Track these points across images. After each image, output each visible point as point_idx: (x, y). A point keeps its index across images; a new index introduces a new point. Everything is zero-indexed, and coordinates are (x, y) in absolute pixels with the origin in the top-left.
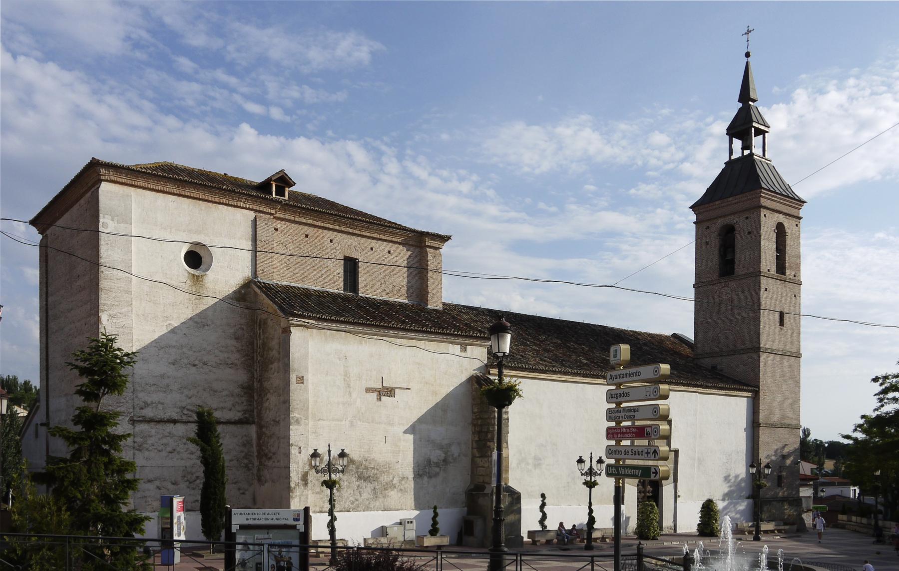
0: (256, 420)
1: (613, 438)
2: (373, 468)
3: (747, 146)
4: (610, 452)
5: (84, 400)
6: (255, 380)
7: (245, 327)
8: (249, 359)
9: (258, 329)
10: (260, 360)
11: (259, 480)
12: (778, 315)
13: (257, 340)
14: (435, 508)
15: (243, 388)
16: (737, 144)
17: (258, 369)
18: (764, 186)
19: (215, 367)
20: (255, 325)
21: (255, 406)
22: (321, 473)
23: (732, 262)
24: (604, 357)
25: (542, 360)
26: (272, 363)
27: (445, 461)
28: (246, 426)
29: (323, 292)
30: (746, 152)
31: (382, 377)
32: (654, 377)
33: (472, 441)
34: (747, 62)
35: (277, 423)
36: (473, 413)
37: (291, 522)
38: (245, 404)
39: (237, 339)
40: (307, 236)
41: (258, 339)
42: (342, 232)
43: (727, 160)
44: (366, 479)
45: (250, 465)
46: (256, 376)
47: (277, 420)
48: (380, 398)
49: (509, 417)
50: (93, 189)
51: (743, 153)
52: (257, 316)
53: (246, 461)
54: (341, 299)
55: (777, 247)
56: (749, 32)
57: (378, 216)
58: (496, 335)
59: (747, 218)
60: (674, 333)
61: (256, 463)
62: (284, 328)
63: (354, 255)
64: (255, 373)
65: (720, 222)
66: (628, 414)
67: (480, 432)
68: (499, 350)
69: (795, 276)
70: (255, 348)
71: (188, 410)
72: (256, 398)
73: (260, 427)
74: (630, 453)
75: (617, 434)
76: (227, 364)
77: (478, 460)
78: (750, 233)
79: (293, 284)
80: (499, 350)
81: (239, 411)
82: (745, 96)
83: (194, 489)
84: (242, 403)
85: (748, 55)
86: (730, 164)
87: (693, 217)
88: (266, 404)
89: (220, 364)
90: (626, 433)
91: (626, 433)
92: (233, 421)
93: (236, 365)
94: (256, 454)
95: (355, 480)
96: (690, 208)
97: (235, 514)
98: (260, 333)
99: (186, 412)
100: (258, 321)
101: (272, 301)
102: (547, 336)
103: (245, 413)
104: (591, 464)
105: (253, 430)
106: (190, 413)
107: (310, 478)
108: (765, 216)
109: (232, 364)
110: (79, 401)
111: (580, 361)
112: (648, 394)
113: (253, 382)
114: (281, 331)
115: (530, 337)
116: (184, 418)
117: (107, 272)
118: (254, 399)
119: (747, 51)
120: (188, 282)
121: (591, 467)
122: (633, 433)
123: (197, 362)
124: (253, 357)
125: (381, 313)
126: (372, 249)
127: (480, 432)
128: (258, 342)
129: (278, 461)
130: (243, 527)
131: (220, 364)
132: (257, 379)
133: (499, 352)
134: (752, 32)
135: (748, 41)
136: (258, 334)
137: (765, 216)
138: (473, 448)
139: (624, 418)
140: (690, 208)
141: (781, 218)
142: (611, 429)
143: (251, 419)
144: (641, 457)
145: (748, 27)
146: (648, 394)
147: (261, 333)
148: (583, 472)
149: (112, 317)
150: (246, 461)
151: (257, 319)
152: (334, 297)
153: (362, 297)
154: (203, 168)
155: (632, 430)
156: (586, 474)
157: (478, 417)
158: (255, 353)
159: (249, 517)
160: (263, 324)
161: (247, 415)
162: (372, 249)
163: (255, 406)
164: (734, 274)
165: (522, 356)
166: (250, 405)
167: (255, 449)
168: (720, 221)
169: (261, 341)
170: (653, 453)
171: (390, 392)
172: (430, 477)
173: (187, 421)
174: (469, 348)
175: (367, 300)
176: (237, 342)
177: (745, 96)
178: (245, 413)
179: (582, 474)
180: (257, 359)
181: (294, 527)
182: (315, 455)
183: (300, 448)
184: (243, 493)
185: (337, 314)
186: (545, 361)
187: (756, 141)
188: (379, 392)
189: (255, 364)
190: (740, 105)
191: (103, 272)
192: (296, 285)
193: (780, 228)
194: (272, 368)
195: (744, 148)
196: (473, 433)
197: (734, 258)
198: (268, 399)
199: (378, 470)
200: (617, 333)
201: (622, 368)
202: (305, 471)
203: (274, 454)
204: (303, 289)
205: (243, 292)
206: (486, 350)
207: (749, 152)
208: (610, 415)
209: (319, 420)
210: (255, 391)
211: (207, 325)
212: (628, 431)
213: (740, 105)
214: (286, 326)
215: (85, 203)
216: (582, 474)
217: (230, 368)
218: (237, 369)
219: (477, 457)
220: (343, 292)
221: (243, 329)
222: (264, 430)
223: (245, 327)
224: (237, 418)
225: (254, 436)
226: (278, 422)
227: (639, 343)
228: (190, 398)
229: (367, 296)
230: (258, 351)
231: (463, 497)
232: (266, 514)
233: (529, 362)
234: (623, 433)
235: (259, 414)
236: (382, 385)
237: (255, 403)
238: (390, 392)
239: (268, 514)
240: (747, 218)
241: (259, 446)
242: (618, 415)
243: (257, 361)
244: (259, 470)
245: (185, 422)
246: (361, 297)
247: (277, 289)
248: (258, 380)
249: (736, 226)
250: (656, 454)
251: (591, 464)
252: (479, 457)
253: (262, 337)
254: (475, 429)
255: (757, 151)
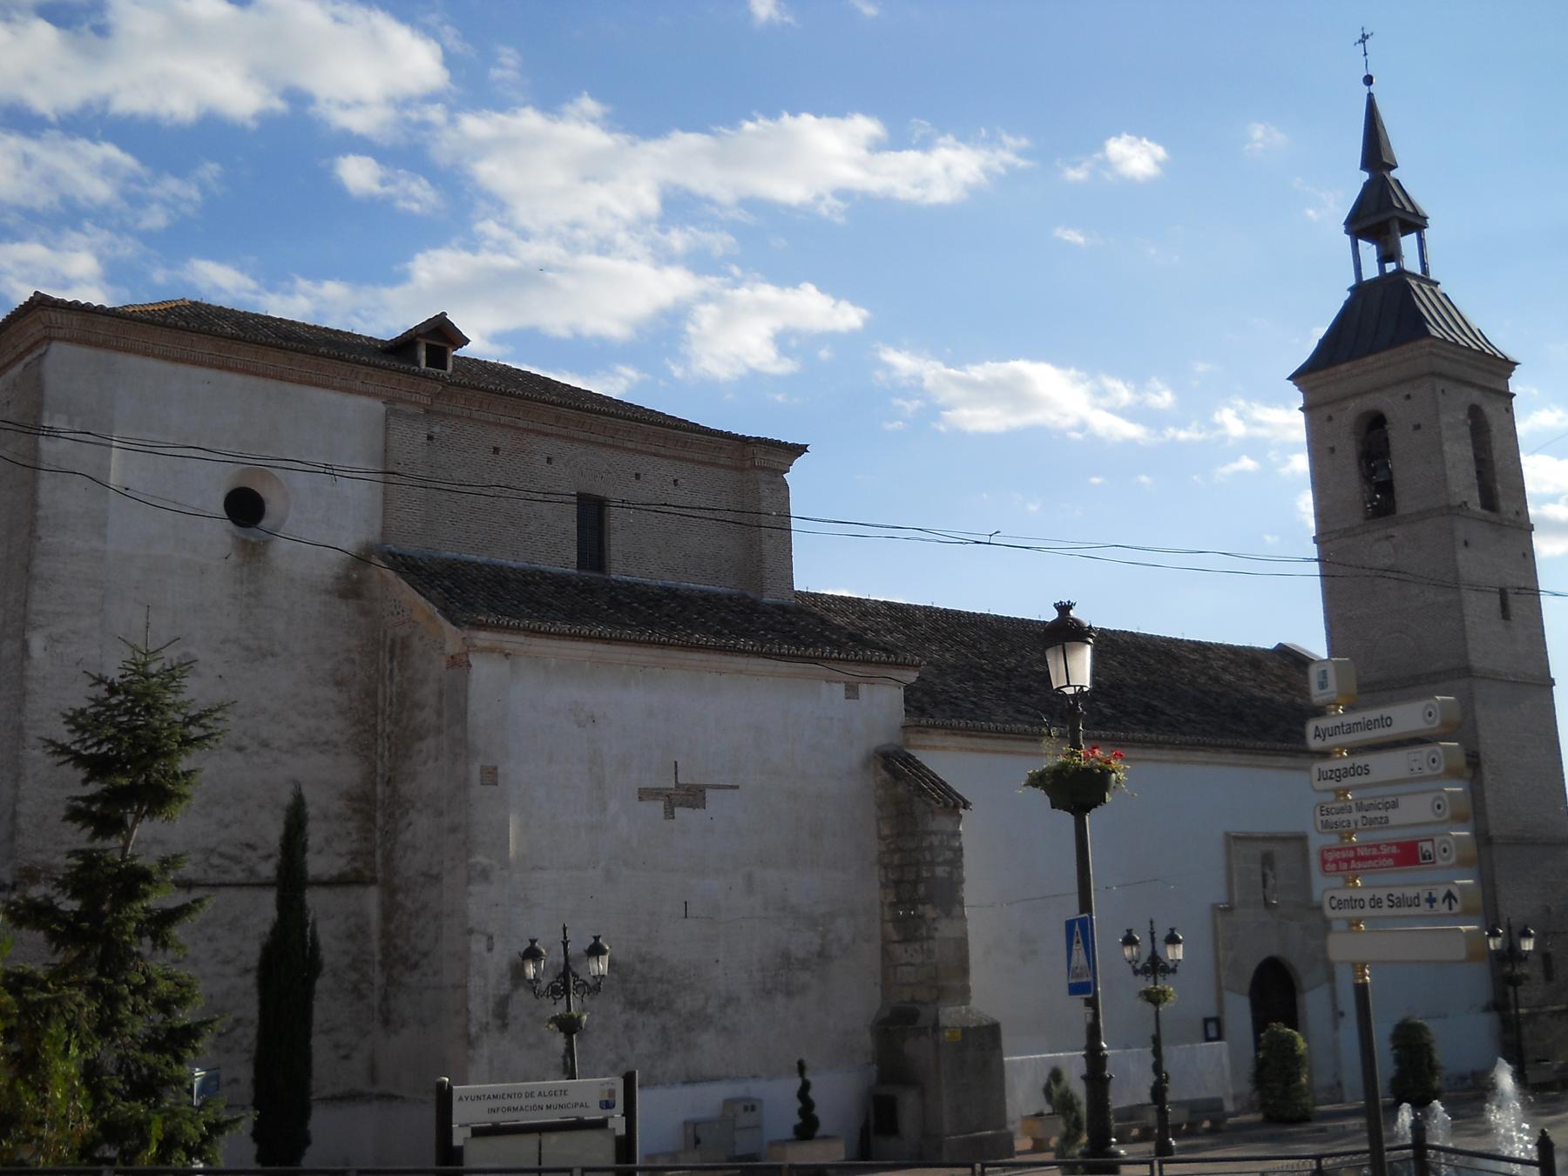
0: (380, 875)
1: (1338, 870)
2: (660, 980)
3: (1389, 254)
4: (1334, 903)
5: (95, 835)
6: (378, 779)
7: (357, 658)
8: (365, 731)
9: (387, 660)
10: (392, 732)
11: (386, 1022)
12: (1496, 600)
13: (385, 686)
14: (801, 1068)
15: (351, 799)
16: (1369, 251)
17: (386, 753)
18: (1434, 333)
19: (287, 752)
20: (381, 653)
21: (379, 841)
22: (548, 997)
23: (1387, 488)
24: (1146, 700)
25: (1019, 712)
26: (421, 739)
27: (823, 955)
28: (357, 891)
29: (533, 573)
30: (1390, 267)
31: (676, 763)
32: (1428, 726)
33: (882, 904)
34: (1370, 95)
35: (433, 879)
36: (881, 838)
37: (594, 1114)
38: (354, 837)
39: (339, 684)
40: (496, 450)
41: (388, 683)
42: (572, 439)
43: (1352, 282)
44: (644, 1006)
45: (363, 986)
46: (380, 771)
47: (434, 871)
48: (673, 813)
49: (963, 844)
50: (28, 359)
51: (1382, 269)
52: (385, 632)
53: (354, 976)
54: (575, 587)
55: (1475, 456)
56: (1365, 38)
57: (646, 407)
58: (1061, 646)
59: (1408, 397)
60: (1280, 644)
61: (378, 978)
62: (452, 657)
63: (598, 490)
64: (379, 763)
65: (1355, 407)
66: (1371, 814)
67: (898, 883)
68: (1068, 682)
69: (1517, 513)
70: (381, 704)
71: (221, 855)
72: (380, 821)
73: (390, 891)
74: (1386, 903)
75: (1348, 860)
76: (315, 744)
77: (898, 950)
78: (1417, 427)
79: (465, 556)
80: (1068, 682)
81: (340, 855)
82: (1376, 154)
83: (228, 1051)
84: (349, 834)
85: (1368, 80)
86: (1361, 290)
87: (1298, 399)
88: (406, 837)
89: (301, 744)
90: (1372, 858)
91: (1372, 858)
92: (325, 878)
93: (336, 746)
94: (378, 957)
95: (617, 1008)
96: (1289, 379)
97: (461, 1099)
98: (391, 671)
99: (215, 860)
100: (388, 642)
101: (424, 596)
102: (1019, 658)
103: (354, 859)
104: (1153, 947)
105: (371, 900)
106: (226, 863)
107: (514, 1010)
108: (1443, 391)
109: (326, 743)
110: (79, 837)
111: (1100, 712)
112: (1416, 766)
113: (374, 784)
114: (444, 664)
115: (983, 661)
116: (213, 876)
117: (50, 540)
118: (375, 826)
119: (1366, 74)
120: (233, 558)
121: (1154, 952)
122: (1388, 856)
123: (245, 742)
124: (375, 726)
125: (668, 615)
126: (638, 476)
127: (898, 883)
128: (388, 690)
129: (435, 973)
130: (478, 1132)
131: (301, 744)
132: (383, 776)
133: (1069, 685)
134: (1357, 41)
135: (1365, 54)
136: (388, 672)
137: (1443, 391)
138: (883, 921)
139: (1360, 823)
140: (1289, 379)
141: (1475, 396)
142: (1329, 851)
143: (367, 873)
144: (1413, 911)
145: (1363, 29)
146: (1416, 766)
147: (396, 671)
148: (1139, 966)
149: (54, 640)
150: (354, 976)
151: (385, 636)
152: (560, 583)
153: (619, 582)
154: (267, 312)
155: (1385, 851)
156: (1144, 971)
157: (892, 846)
158: (379, 717)
159: (493, 1104)
160: (399, 649)
161: (358, 865)
162: (638, 476)
163: (379, 841)
164: (1395, 513)
165: (973, 703)
166: (366, 839)
167: (375, 945)
168: (1353, 405)
169: (394, 689)
170: (1444, 901)
171: (693, 796)
172: (789, 994)
173: (217, 882)
174: (863, 688)
175: (631, 587)
176: (341, 691)
177: (1376, 154)
178: (354, 859)
179: (1136, 972)
180: (384, 731)
181: (601, 1125)
182: (532, 954)
183: (490, 938)
184: (347, 1057)
185: (571, 617)
186: (1027, 713)
187: (1408, 243)
188: (668, 796)
189: (380, 742)
190: (1366, 176)
191: (40, 538)
192: (473, 557)
193: (1475, 412)
194: (421, 751)
195: (1384, 258)
196: (884, 886)
197: (1391, 480)
198: (410, 824)
199: (669, 982)
200: (1163, 646)
201: (1341, 712)
202: (502, 993)
203: (425, 955)
204: (488, 566)
205: (355, 576)
206: (899, 694)
207: (1395, 268)
208: (1324, 818)
209: (533, 869)
210: (379, 804)
211: (272, 655)
212: (1375, 852)
213: (1366, 176)
214: (457, 651)
215: (7, 390)
216: (1136, 972)
217: (321, 752)
218: (338, 754)
219: (894, 942)
220: (575, 571)
221: (353, 661)
222: (400, 897)
223: (357, 658)
224: (335, 872)
225: (374, 912)
226: (437, 878)
227: (1211, 667)
228: (227, 826)
229: (628, 578)
230: (388, 713)
231: (867, 1041)
232: (536, 1094)
233: (993, 717)
234: (1363, 859)
235: (388, 858)
236: (676, 782)
237: (378, 834)
238: (693, 796)
239: (540, 1094)
240: (1408, 397)
241: (386, 935)
242: (1344, 817)
243: (385, 735)
244: (385, 998)
245: (214, 885)
246: (616, 581)
247: (431, 568)
248: (386, 779)
249: (1389, 415)
250: (1453, 901)
251: (1153, 947)
252: (898, 942)
253: (397, 679)
254: (887, 876)
255: (1411, 263)
